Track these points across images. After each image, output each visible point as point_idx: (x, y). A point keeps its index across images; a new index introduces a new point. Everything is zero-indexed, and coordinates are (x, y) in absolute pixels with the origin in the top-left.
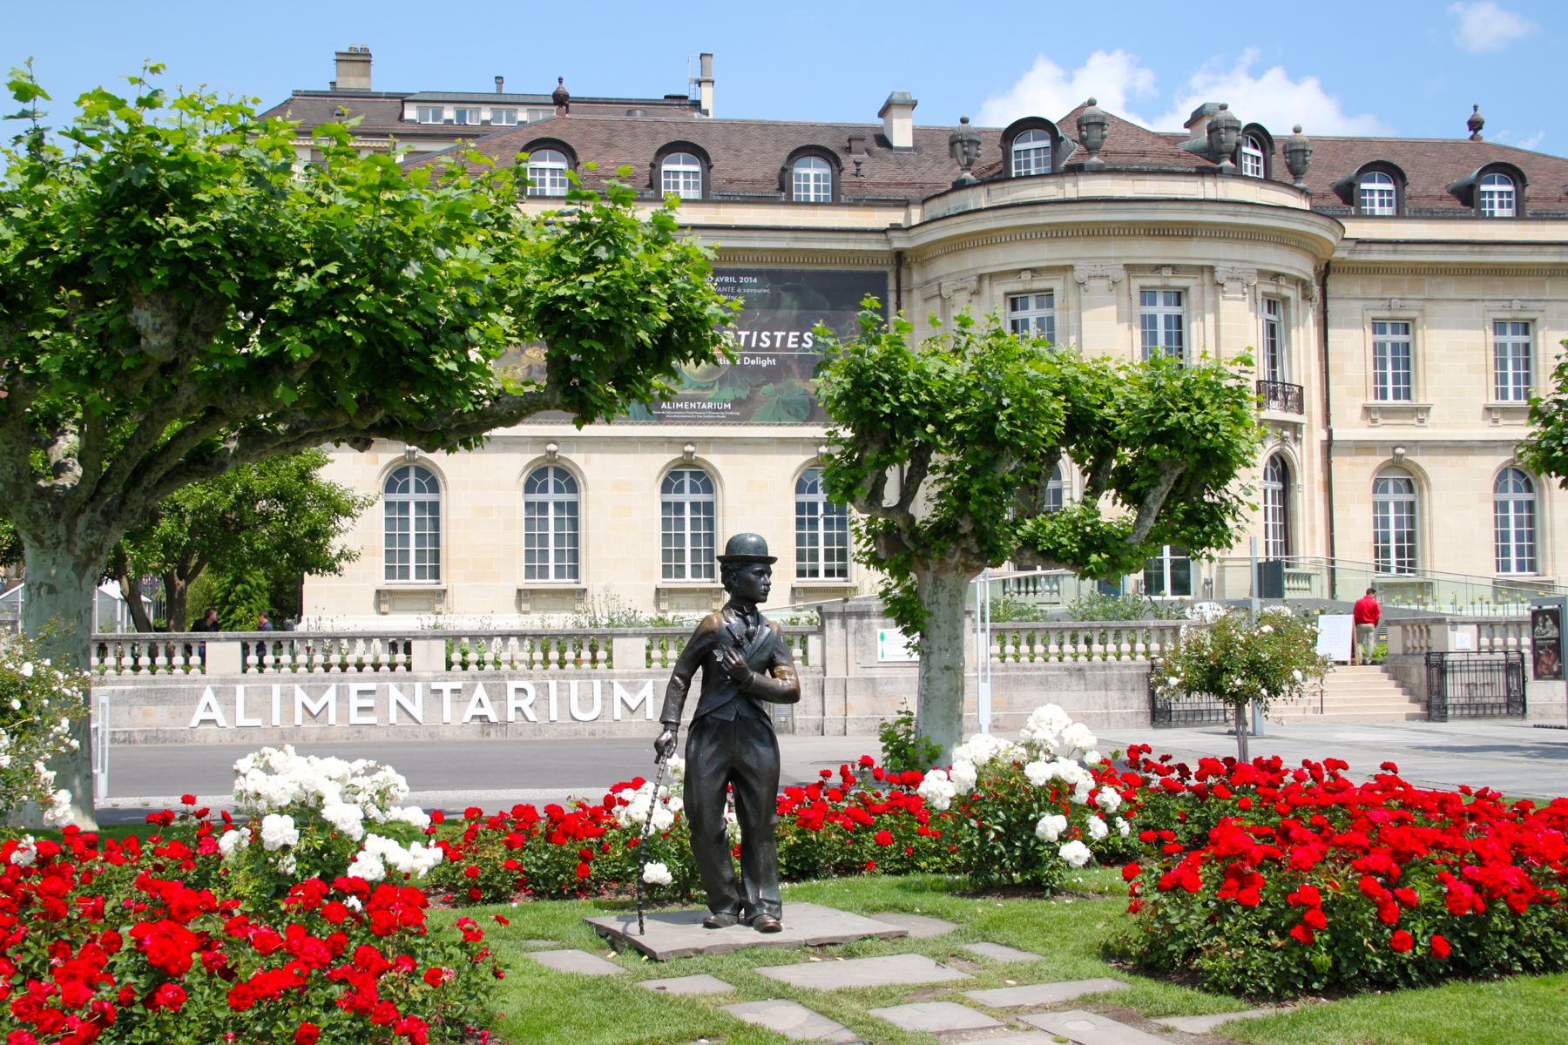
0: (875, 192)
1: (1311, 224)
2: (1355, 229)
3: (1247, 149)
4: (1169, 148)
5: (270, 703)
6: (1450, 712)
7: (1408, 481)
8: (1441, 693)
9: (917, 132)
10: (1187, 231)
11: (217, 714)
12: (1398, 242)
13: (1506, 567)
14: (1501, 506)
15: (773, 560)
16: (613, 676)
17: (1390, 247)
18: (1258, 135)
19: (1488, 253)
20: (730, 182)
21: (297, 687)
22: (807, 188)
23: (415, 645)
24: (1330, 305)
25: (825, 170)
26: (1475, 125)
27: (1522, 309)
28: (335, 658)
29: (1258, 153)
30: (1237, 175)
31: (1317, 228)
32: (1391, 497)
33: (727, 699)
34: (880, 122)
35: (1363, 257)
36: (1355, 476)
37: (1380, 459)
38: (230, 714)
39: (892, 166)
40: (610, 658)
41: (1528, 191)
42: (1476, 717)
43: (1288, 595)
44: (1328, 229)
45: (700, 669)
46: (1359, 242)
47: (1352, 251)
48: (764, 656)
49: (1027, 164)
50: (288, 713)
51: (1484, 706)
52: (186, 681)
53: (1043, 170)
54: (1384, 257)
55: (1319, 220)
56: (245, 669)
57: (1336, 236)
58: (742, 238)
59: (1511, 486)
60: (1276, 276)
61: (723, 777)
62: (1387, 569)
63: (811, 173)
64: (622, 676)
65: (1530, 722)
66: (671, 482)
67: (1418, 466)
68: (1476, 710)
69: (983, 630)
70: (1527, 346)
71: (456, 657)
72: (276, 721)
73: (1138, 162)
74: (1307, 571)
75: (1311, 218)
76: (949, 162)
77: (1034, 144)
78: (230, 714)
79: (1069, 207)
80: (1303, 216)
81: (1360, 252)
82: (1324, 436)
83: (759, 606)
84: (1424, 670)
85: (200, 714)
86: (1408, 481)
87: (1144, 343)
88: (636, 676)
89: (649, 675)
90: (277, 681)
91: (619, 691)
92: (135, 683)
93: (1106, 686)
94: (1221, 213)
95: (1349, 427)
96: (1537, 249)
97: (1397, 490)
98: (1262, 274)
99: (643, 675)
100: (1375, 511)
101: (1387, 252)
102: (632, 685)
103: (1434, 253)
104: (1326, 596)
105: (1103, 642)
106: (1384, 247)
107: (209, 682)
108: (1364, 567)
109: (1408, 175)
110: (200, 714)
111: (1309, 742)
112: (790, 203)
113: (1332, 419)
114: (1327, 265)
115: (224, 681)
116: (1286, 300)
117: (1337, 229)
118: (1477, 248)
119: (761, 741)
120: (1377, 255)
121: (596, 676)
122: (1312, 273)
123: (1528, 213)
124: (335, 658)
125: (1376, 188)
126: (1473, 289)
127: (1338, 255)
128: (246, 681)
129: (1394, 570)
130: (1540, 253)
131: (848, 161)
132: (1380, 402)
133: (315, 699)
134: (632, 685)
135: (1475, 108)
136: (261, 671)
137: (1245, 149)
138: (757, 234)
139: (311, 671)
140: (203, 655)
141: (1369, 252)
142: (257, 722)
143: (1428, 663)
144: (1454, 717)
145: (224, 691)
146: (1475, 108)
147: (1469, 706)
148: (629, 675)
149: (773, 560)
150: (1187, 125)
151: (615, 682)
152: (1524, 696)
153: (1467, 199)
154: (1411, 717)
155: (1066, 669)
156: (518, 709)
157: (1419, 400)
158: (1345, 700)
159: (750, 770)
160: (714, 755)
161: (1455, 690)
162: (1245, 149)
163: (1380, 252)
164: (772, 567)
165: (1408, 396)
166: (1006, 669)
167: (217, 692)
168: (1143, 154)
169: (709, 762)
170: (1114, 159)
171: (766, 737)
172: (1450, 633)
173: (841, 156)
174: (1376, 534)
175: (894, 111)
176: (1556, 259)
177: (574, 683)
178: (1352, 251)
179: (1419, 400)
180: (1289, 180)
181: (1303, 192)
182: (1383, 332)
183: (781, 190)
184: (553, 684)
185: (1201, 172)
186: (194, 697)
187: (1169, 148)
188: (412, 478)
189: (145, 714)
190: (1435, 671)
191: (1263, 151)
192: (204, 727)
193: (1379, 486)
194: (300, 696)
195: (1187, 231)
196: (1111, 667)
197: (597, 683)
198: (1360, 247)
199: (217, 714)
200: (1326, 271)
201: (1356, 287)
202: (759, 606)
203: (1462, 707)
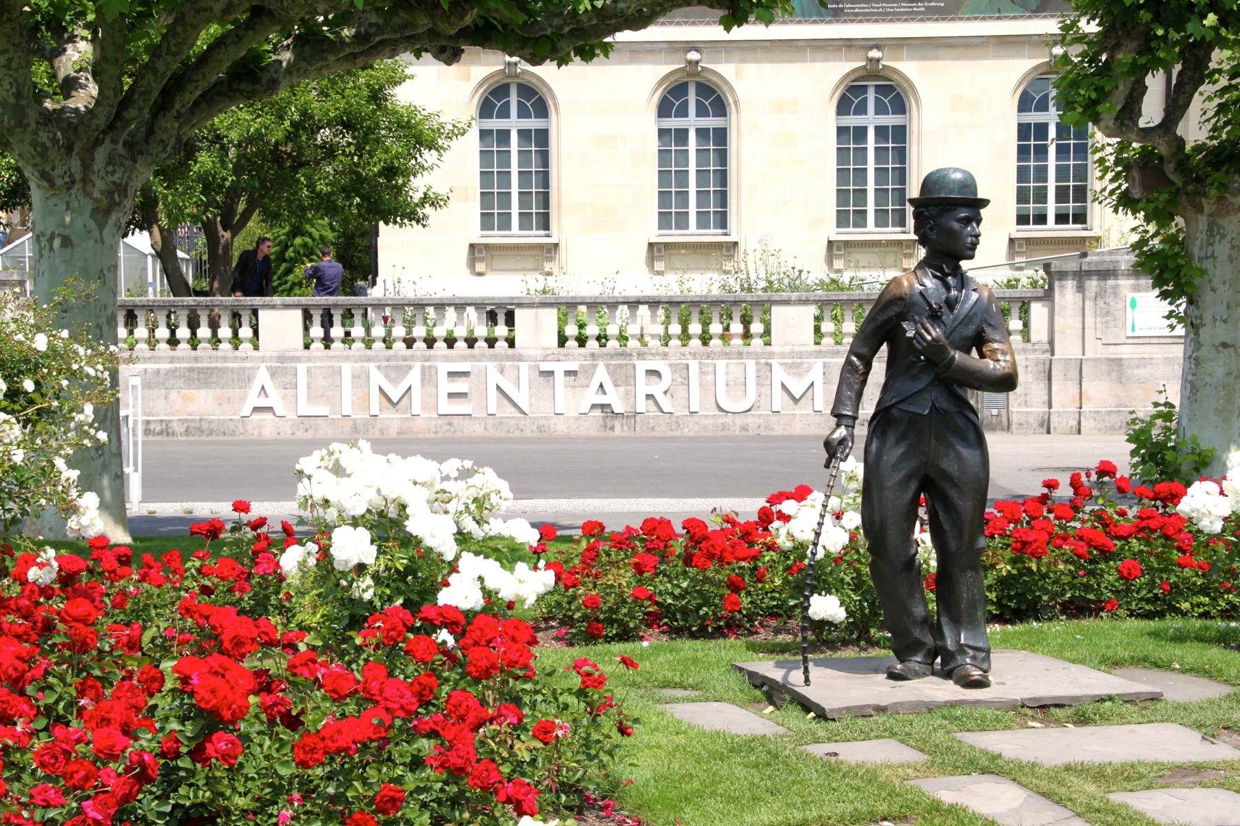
15: (984, 203)
33: (920, 385)
40: (767, 332)
45: (884, 347)
48: (970, 330)
56: (562, 340)
61: (913, 486)
64: (783, 355)
66: (849, 99)
71: (571, 330)
83: (965, 264)
85: (254, 400)
88: (801, 355)
89: (819, 354)
91: (779, 374)
92: (172, 360)
107: (263, 360)
115: (282, 358)
119: (964, 440)
124: (419, 331)
128: (309, 359)
133: (395, 382)
134: (796, 368)
145: (282, 369)
148: (791, 354)
149: (984, 203)
151: (774, 362)
164: (983, 212)
167: (273, 373)
169: (895, 467)
171: (972, 436)
177: (721, 364)
184: (694, 365)
186: (245, 378)
188: (514, 99)
189: (186, 399)
202: (965, 264)
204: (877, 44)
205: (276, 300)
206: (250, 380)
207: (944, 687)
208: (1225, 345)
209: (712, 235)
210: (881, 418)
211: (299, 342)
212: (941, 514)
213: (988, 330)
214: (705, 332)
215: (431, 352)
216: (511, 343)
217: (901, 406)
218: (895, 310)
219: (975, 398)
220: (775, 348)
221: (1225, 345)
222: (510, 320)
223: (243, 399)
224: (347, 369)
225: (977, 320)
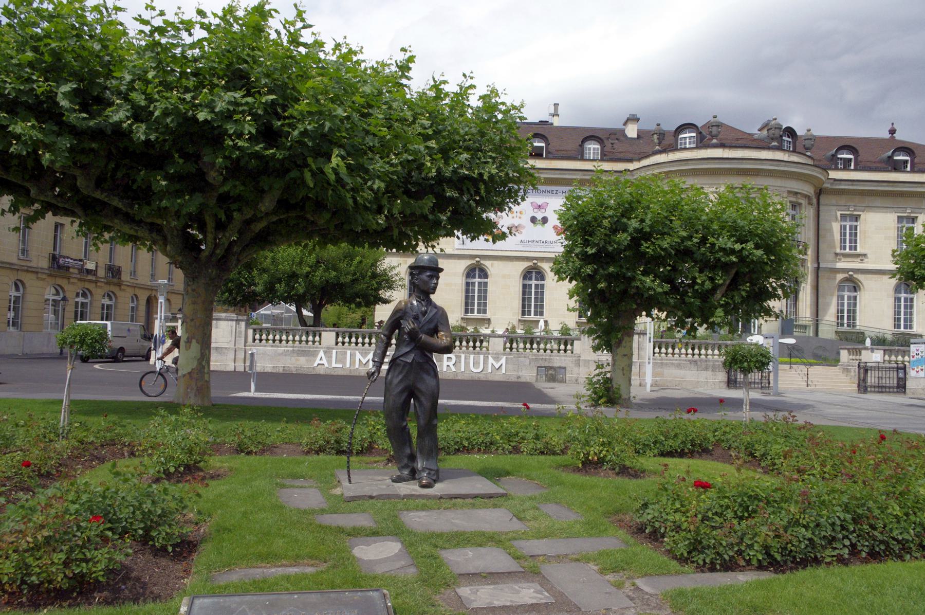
0: (619, 156)
1: (813, 171)
2: (833, 174)
5: (346, 358)
6: (869, 389)
8: (865, 380)
10: (756, 173)
11: (324, 361)
13: (899, 327)
14: (898, 300)
15: (441, 270)
16: (489, 354)
17: (850, 183)
18: (790, 132)
19: (896, 187)
20: (558, 151)
21: (357, 352)
22: (590, 153)
24: (821, 208)
25: (598, 146)
26: (892, 132)
27: (912, 212)
29: (790, 140)
31: (816, 173)
33: (408, 349)
34: (624, 127)
35: (837, 187)
38: (330, 362)
42: (882, 392)
44: (820, 173)
45: (397, 331)
46: (835, 180)
47: (832, 184)
48: (432, 326)
49: (685, 143)
50: (352, 362)
51: (885, 387)
53: (692, 146)
54: (847, 187)
55: (817, 169)
56: (337, 343)
57: (825, 177)
58: (561, 174)
59: (903, 291)
60: (796, 193)
61: (405, 394)
62: (842, 325)
63: (593, 148)
64: (493, 354)
65: (907, 396)
66: (527, 275)
67: (856, 279)
68: (881, 389)
72: (348, 366)
73: (735, 143)
75: (813, 168)
77: (688, 135)
78: (330, 362)
79: (703, 161)
80: (810, 167)
81: (836, 185)
82: (816, 265)
83: (432, 296)
85: (318, 361)
86: (854, 287)
88: (498, 354)
89: (504, 354)
90: (349, 349)
91: (491, 360)
92: (293, 347)
93: (706, 369)
94: (771, 165)
96: (920, 185)
98: (789, 192)
99: (502, 354)
101: (849, 185)
102: (497, 359)
103: (871, 186)
105: (706, 349)
106: (847, 183)
107: (322, 348)
108: (831, 323)
110: (318, 361)
112: (582, 159)
113: (820, 258)
114: (820, 190)
115: (328, 348)
116: (800, 204)
117: (825, 173)
118: (891, 184)
119: (429, 374)
120: (843, 187)
121: (482, 354)
122: (813, 193)
123: (916, 169)
126: (887, 202)
127: (826, 185)
128: (337, 349)
129: (845, 325)
130: (920, 187)
131: (608, 143)
132: (842, 251)
133: (364, 357)
134: (497, 359)
135: (893, 124)
137: (784, 138)
138: (567, 172)
140: (320, 336)
141: (840, 184)
142: (340, 366)
143: (859, 366)
144: (871, 392)
145: (328, 352)
146: (893, 124)
147: (878, 387)
148: (496, 354)
149: (441, 270)
150: (759, 130)
151: (490, 356)
152: (905, 384)
155: (689, 361)
156: (448, 366)
157: (859, 250)
159: (421, 391)
160: (401, 381)
161: (871, 379)
162: (784, 138)
163: (845, 185)
164: (440, 274)
166: (662, 360)
167: (325, 353)
169: (396, 385)
171: (432, 373)
175: (629, 122)
177: (472, 356)
178: (832, 184)
183: (579, 156)
184: (463, 356)
186: (315, 354)
189: (297, 360)
190: (862, 371)
192: (319, 367)
194: (358, 356)
195: (756, 173)
196: (709, 361)
197: (482, 357)
198: (836, 182)
199: (324, 361)
200: (820, 192)
201: (833, 200)
202: (432, 296)
203: (875, 387)
204: (536, 258)
205: (328, 329)
206: (317, 355)
208: (625, 355)
209: (481, 316)
210: (393, 362)
211: (334, 342)
212: (418, 408)
217: (401, 359)
218: (399, 315)
219: (435, 357)
221: (625, 355)
223: (315, 361)
224: (349, 352)
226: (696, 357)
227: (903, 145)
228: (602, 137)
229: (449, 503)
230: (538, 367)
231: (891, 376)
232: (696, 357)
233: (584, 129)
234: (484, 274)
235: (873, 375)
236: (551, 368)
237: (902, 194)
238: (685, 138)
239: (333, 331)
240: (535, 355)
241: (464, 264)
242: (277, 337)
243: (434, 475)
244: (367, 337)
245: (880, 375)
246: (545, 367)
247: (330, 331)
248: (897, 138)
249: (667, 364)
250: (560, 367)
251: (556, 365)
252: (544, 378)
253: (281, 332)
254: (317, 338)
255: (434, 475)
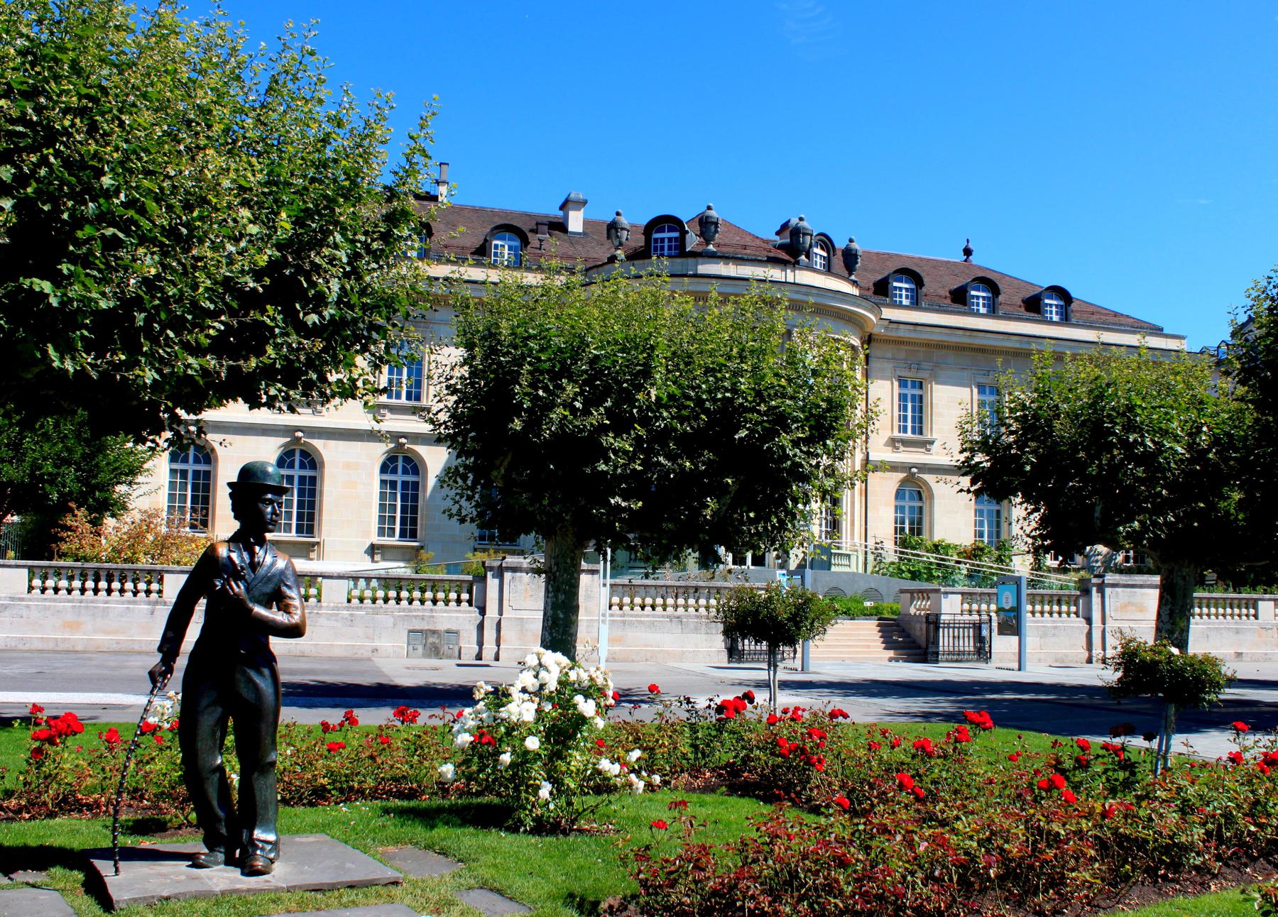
2: (888, 313)
3: (817, 250)
4: (763, 245)
7: (919, 492)
9: (586, 223)
12: (917, 324)
18: (826, 242)
23: (166, 576)
28: (649, 601)
30: (810, 268)
32: (907, 504)
36: (884, 487)
37: (902, 475)
39: (567, 245)
40: (319, 594)
41: (1001, 298)
43: (833, 569)
46: (891, 322)
48: (269, 588)
52: (632, 616)
56: (31, 588)
57: (876, 317)
69: (605, 585)
70: (921, 397)
71: (616, 600)
74: (848, 552)
75: (860, 301)
76: (608, 244)
84: (924, 626)
87: (900, 400)
95: (880, 453)
97: (912, 498)
100: (896, 512)
104: (861, 570)
109: (926, 280)
111: (621, 671)
120: (903, 333)
124: (649, 601)
125: (902, 286)
132: (902, 435)
136: (398, 603)
139: (654, 609)
150: (778, 233)
153: (959, 298)
154: (890, 660)
157: (927, 436)
158: (850, 646)
165: (921, 433)
168: (745, 247)
170: (725, 249)
172: (943, 600)
173: (530, 235)
174: (896, 528)
176: (1018, 345)
179: (927, 436)
180: (846, 273)
181: (854, 283)
182: (906, 386)
183: (481, 253)
185: (773, 261)
187: (763, 245)
188: (400, 464)
190: (932, 626)
191: (828, 252)
193: (899, 495)
201: (889, 351)
207: (177, 869)
209: (917, 437)
213: (284, 589)
214: (434, 596)
215: (109, 598)
216: (160, 592)
220: (324, 604)
222: (161, 581)
225: (275, 580)
226: (681, 610)
227: (980, 274)
228: (525, 229)
229: (349, 895)
230: (410, 631)
231: (956, 634)
232: (681, 610)
233: (493, 213)
234: (311, 461)
235: (951, 634)
236: (434, 632)
237: (982, 350)
238: (662, 240)
239: (24, 567)
240: (404, 610)
241: (378, 451)
242: (638, 600)
243: (271, 851)
244: (91, 577)
245: (956, 634)
246: (421, 631)
247: (18, 566)
248: (974, 263)
249: (631, 623)
250: (448, 632)
251: (442, 626)
252: (420, 648)
253: (58, 573)
254: (155, 586)
255: (271, 851)
